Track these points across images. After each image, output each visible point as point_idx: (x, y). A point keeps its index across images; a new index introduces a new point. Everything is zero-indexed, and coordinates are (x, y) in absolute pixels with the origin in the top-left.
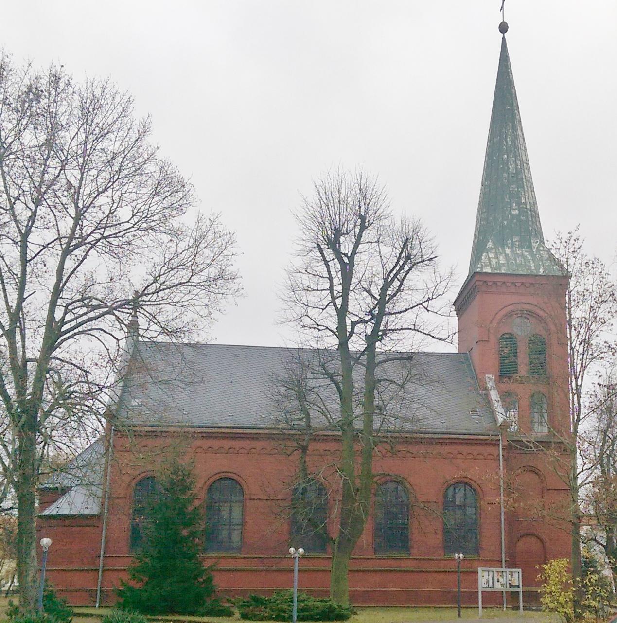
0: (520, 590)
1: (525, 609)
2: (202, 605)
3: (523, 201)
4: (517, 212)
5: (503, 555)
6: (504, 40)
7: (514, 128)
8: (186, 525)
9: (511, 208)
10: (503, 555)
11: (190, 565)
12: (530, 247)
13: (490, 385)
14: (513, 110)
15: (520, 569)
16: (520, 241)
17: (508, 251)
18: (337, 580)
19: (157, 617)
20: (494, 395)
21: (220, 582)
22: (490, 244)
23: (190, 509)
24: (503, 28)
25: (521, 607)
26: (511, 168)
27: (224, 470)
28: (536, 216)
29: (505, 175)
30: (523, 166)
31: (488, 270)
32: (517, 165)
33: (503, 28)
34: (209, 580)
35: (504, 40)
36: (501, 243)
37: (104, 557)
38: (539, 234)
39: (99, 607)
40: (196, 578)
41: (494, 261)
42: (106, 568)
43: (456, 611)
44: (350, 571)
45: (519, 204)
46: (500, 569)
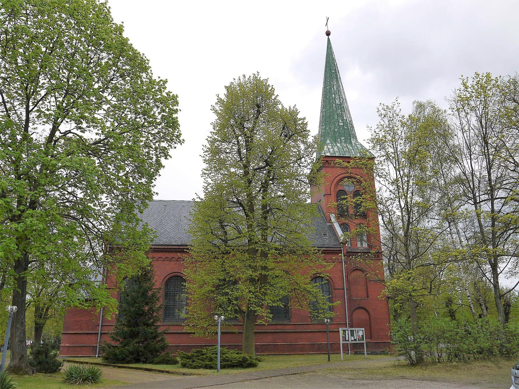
0: (364, 341)
1: (368, 354)
2: (157, 356)
3: (345, 118)
4: (342, 124)
5: (347, 321)
6: (329, 39)
7: (337, 81)
8: (147, 304)
9: (338, 122)
10: (347, 321)
11: (150, 330)
12: (351, 143)
13: (333, 220)
14: (336, 72)
15: (363, 329)
16: (345, 139)
17: (339, 145)
18: (247, 338)
19: (124, 365)
20: (337, 226)
21: (169, 341)
22: (328, 141)
23: (150, 293)
24: (328, 34)
25: (365, 352)
26: (337, 102)
27: (175, 271)
28: (353, 127)
29: (334, 105)
30: (334, 59)
31: (328, 154)
32: (340, 99)
33: (328, 34)
34: (162, 340)
35: (329, 39)
36: (335, 140)
37: (102, 326)
38: (355, 137)
39: (98, 357)
40: (154, 338)
41: (331, 150)
42: (102, 332)
43: (327, 356)
44: (256, 333)
45: (343, 120)
46: (344, 329)
